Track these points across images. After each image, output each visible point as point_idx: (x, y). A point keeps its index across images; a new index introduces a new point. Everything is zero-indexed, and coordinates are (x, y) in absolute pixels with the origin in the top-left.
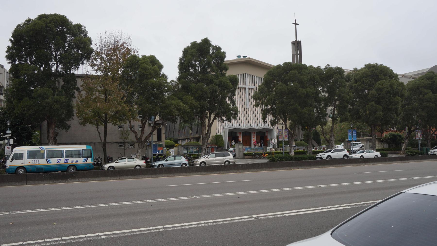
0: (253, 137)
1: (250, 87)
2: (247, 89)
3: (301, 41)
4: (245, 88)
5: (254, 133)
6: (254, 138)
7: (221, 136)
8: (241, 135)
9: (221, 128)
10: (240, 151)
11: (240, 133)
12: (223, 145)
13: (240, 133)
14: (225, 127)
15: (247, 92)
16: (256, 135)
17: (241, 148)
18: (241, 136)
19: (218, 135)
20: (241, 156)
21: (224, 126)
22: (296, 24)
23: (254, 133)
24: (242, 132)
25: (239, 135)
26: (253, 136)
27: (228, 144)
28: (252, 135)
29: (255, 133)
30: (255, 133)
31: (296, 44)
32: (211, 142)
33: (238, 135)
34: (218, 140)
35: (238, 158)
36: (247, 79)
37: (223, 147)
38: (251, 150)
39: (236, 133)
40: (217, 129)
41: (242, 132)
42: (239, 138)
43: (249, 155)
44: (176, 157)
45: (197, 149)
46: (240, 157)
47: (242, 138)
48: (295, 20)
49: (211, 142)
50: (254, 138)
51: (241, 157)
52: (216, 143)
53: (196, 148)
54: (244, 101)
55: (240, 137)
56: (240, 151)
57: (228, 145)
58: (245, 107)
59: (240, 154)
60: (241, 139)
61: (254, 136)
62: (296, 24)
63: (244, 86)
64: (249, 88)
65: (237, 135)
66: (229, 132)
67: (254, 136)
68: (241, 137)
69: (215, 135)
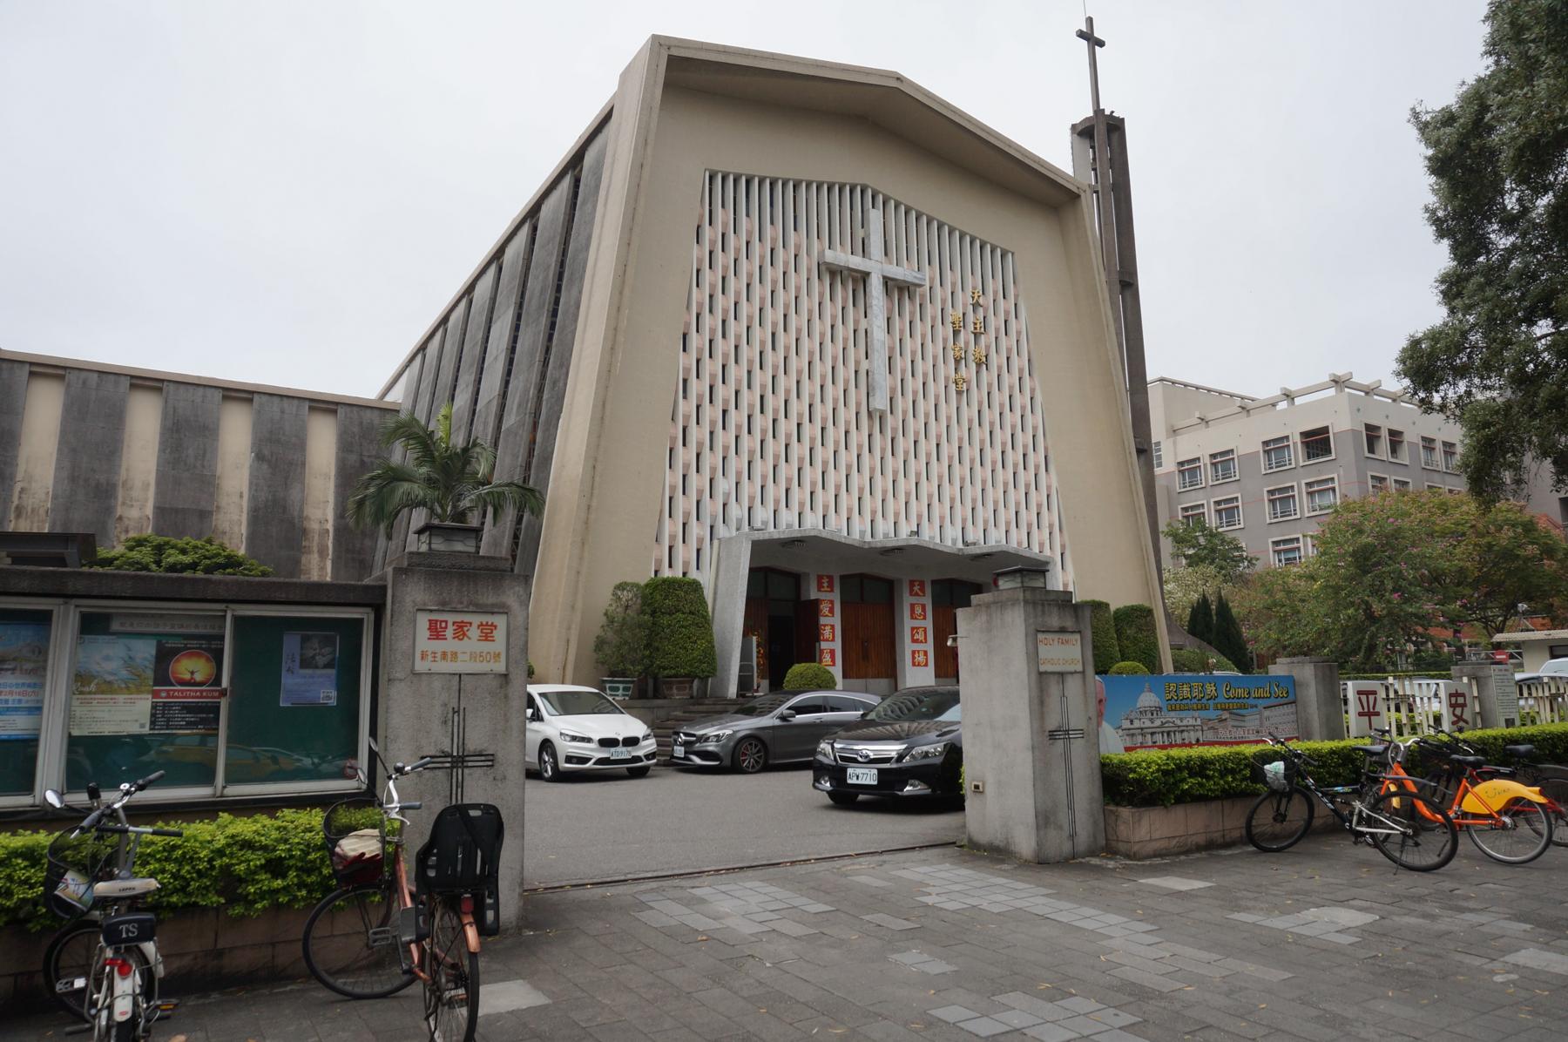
0: (912, 611)
1: (902, 272)
2: (876, 285)
3: (1123, 119)
4: (863, 278)
5: (916, 588)
6: (916, 623)
7: (696, 587)
8: (836, 597)
9: (695, 530)
10: (1052, 735)
11: (825, 581)
12: (708, 664)
13: (825, 581)
14: (722, 531)
15: (874, 302)
16: (927, 601)
17: (1062, 675)
18: (832, 602)
19: (671, 584)
20: (1063, 817)
21: (714, 518)
22: (1091, 39)
23: (916, 588)
24: (842, 577)
25: (821, 596)
26: (912, 606)
27: (745, 654)
28: (907, 600)
29: (922, 589)
30: (922, 584)
31: (1100, 133)
32: (610, 635)
33: (814, 594)
34: (665, 620)
35: (1025, 843)
36: (875, 216)
37: (704, 680)
38: (1173, 717)
39: (796, 579)
40: (688, 307)
41: (842, 577)
42: (823, 620)
43: (1184, 798)
44: (1078, 636)
45: (162, 677)
46: (1058, 843)
47: (836, 620)
48: (1090, 21)
49: (610, 635)
50: (916, 623)
51: (1072, 837)
52: (647, 646)
53: (145, 651)
54: (857, 363)
55: (825, 608)
56: (1053, 722)
57: (742, 668)
58: (858, 404)
59: (1058, 776)
60: (833, 627)
61: (918, 610)
62: (1091, 39)
63: (856, 262)
64: (887, 282)
65: (803, 598)
66: (752, 570)
67: (918, 610)
68: (832, 611)
69: (643, 582)
